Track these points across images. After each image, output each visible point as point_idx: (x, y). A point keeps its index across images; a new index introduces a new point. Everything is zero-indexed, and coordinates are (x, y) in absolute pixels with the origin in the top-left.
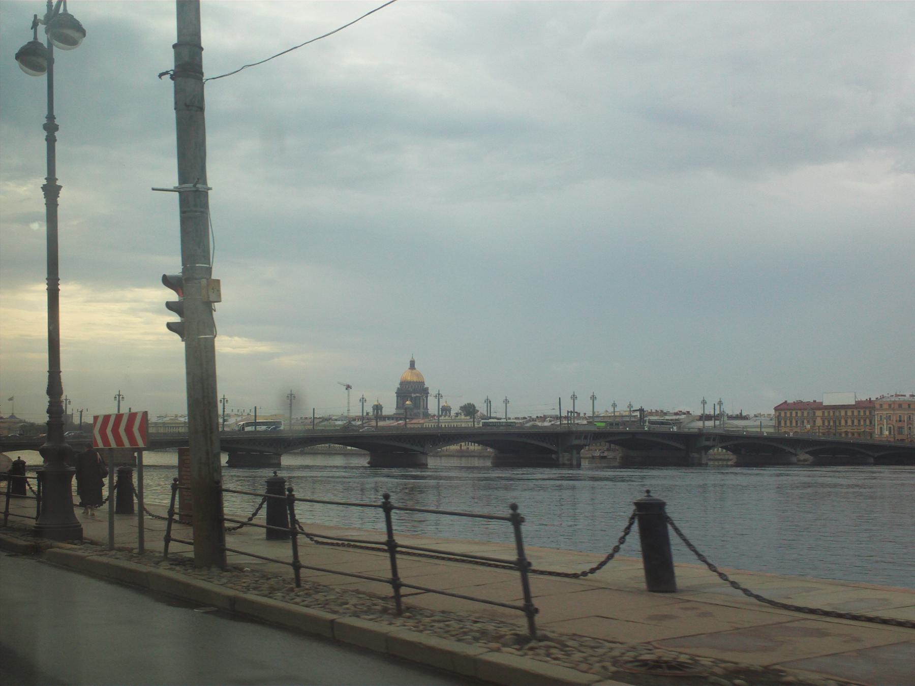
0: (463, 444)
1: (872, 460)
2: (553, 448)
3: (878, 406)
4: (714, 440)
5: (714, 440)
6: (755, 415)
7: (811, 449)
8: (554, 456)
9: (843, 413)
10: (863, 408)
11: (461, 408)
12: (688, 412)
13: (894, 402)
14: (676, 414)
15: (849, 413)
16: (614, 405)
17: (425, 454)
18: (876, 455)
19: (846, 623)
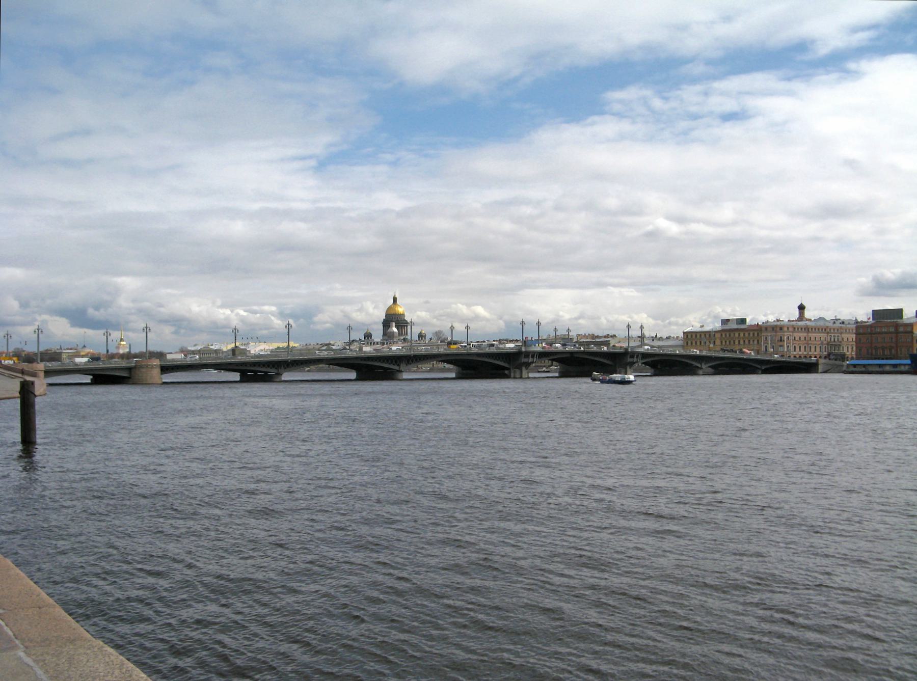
0: (435, 362)
1: (760, 372)
2: (506, 365)
3: (764, 329)
4: (533, 357)
5: (533, 357)
6: (22, 370)
7: (713, 364)
8: (506, 372)
9: (737, 335)
10: (754, 330)
11: (433, 334)
12: (615, 335)
13: (776, 326)
14: (605, 337)
15: (742, 334)
16: (556, 330)
17: (400, 371)
18: (763, 368)
19: (300, 378)
